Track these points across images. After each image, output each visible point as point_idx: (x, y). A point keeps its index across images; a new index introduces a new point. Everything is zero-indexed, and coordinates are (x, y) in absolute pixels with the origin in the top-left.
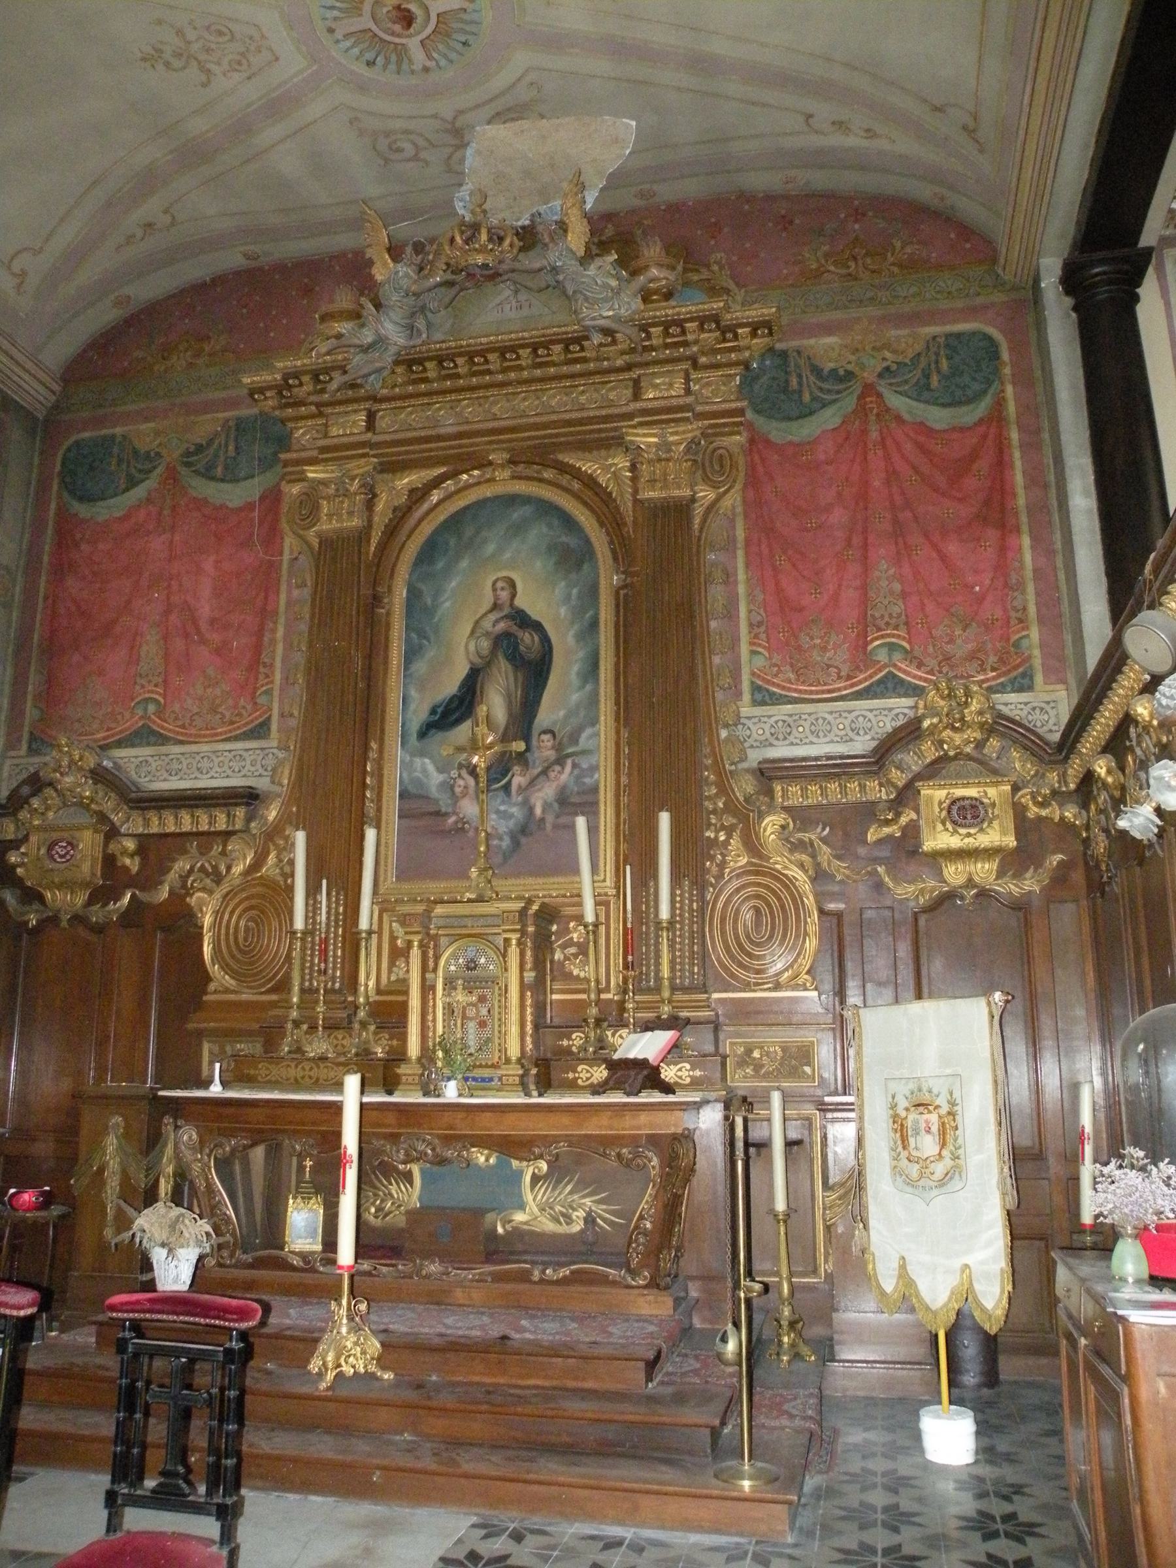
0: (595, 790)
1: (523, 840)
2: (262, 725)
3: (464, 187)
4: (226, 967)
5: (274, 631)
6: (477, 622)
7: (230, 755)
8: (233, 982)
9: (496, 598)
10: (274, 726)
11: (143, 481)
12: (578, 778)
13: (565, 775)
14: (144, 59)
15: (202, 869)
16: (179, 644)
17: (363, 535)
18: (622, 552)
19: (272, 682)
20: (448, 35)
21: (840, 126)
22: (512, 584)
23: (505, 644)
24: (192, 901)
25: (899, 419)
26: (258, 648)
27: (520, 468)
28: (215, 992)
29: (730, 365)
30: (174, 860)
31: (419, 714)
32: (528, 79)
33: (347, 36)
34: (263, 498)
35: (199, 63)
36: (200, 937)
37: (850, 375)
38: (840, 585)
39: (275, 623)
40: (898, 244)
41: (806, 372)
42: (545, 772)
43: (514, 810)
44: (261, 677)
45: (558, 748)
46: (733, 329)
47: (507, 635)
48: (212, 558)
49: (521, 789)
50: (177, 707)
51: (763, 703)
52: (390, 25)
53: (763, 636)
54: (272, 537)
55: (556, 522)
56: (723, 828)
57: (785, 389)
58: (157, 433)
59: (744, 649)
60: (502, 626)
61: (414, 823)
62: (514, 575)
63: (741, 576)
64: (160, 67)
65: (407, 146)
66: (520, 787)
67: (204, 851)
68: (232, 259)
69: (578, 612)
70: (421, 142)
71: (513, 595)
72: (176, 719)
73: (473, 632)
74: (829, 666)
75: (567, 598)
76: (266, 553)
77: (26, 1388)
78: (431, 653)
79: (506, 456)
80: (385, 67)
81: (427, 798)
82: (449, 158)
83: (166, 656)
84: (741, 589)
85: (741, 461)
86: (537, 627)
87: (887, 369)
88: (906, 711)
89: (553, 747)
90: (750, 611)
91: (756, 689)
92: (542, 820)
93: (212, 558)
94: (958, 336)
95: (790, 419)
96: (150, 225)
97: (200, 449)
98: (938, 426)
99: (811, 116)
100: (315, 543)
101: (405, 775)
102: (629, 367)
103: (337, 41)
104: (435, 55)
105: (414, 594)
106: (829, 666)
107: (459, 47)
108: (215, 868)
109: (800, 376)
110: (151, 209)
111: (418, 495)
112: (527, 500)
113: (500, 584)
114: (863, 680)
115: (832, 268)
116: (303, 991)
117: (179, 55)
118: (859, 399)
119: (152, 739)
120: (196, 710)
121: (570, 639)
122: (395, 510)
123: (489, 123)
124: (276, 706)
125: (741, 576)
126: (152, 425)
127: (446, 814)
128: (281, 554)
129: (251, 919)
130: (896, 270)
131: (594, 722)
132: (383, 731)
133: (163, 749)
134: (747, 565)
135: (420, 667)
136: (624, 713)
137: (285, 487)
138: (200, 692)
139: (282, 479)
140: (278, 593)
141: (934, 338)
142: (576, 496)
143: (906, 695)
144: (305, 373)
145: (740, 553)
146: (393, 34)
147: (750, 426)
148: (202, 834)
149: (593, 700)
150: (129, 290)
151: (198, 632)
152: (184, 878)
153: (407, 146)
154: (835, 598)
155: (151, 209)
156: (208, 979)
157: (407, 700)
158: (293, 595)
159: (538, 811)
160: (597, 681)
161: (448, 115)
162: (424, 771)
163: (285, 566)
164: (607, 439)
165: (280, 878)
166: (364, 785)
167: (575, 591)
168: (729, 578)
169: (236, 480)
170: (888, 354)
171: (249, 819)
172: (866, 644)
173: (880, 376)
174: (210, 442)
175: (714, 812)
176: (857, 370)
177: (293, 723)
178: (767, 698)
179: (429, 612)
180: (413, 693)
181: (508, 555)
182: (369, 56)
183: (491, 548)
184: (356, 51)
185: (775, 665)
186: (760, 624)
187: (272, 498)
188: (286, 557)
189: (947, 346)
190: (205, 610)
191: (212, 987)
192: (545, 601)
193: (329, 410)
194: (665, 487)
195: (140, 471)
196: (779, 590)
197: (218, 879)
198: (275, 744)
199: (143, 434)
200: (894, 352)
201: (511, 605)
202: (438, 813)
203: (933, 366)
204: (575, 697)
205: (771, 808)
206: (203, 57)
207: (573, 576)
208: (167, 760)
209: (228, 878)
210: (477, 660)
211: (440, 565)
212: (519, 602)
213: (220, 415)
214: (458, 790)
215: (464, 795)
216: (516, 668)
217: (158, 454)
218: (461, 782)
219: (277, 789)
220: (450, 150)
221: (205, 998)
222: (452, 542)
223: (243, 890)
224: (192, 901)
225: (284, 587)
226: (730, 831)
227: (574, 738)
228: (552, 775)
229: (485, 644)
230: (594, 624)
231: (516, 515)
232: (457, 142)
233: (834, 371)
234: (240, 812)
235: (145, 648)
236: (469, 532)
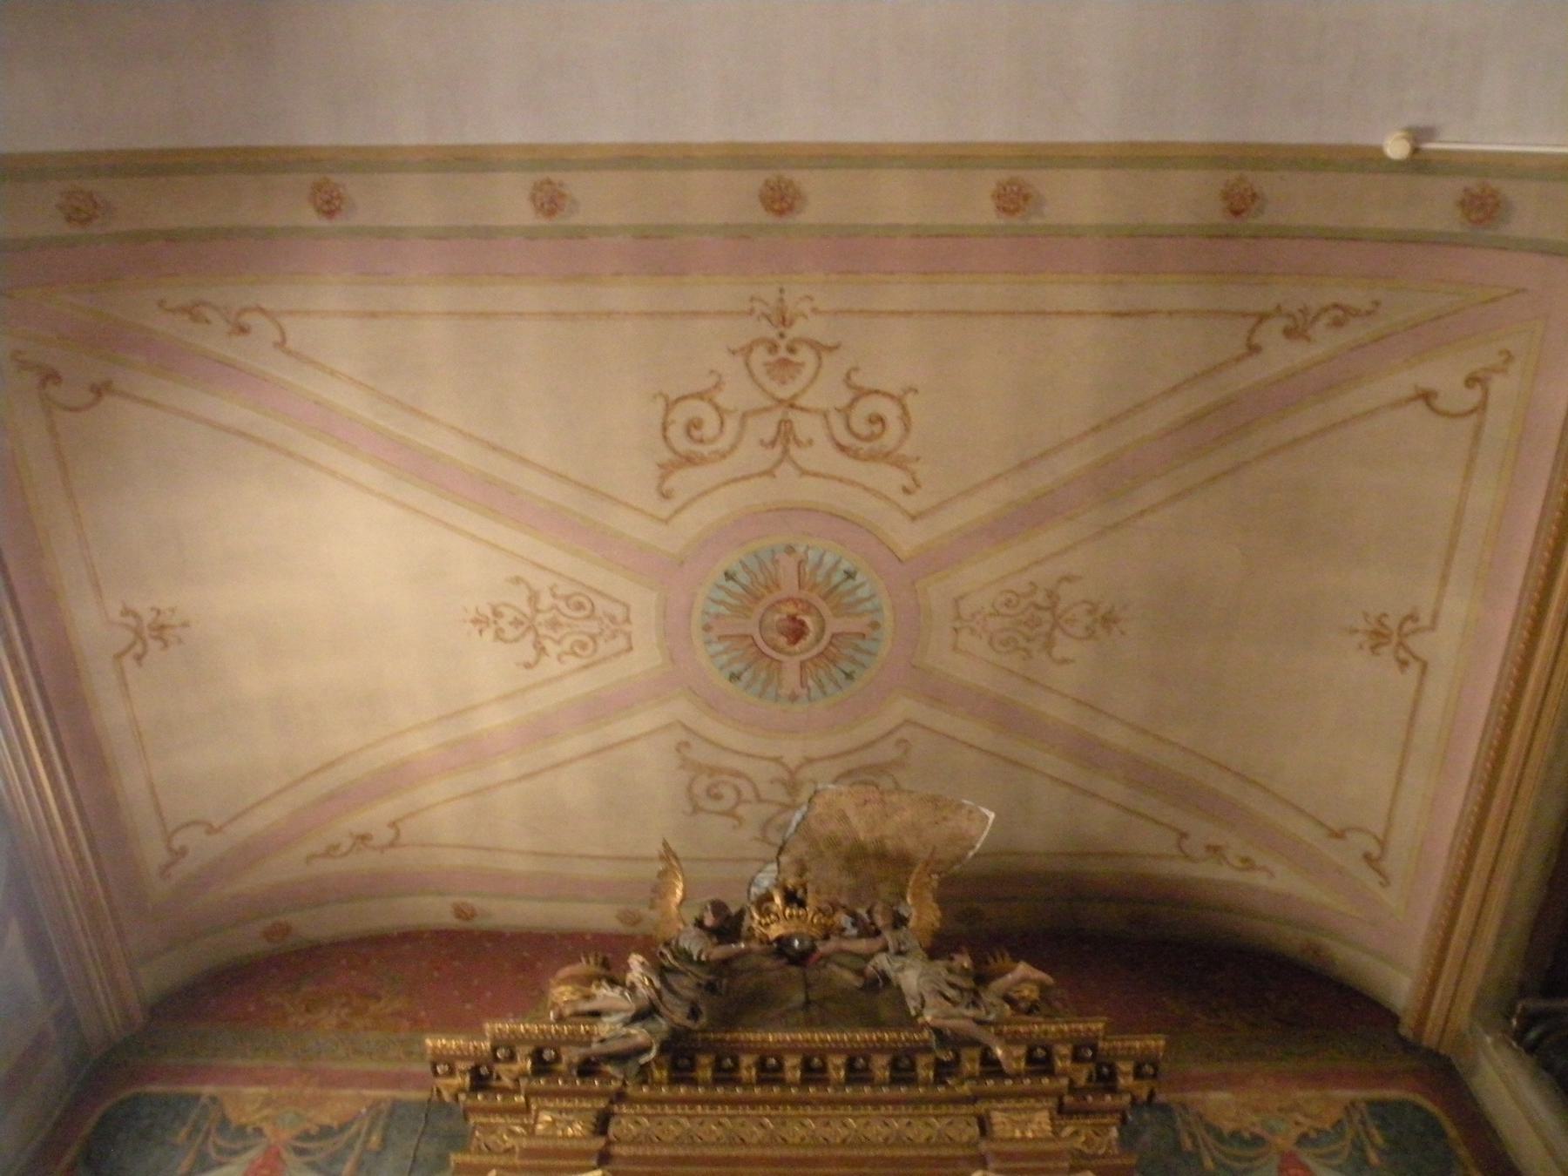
11: (221, 1164)
14: (475, 621)
20: (834, 662)
32: (898, 736)
33: (721, 638)
35: (537, 635)
37: (1257, 1141)
41: (1200, 1132)
52: (775, 635)
57: (1177, 1147)
64: (489, 634)
65: (728, 793)
70: (748, 793)
77: (143, 146)
80: (748, 686)
96: (364, 838)
97: (326, 1132)
102: (973, 1099)
103: (708, 643)
104: (811, 683)
107: (840, 677)
109: (1192, 1136)
117: (516, 623)
123: (835, 781)
126: (263, 1090)
141: (1353, 1104)
146: (775, 648)
153: (728, 793)
170: (1301, 1119)
174: (343, 1128)
176: (1265, 1134)
182: (737, 667)
184: (725, 658)
195: (220, 1151)
203: (1363, 1136)
206: (542, 631)
213: (366, 1092)
217: (259, 1131)
220: (773, 809)
232: (787, 800)
233: (1235, 1135)
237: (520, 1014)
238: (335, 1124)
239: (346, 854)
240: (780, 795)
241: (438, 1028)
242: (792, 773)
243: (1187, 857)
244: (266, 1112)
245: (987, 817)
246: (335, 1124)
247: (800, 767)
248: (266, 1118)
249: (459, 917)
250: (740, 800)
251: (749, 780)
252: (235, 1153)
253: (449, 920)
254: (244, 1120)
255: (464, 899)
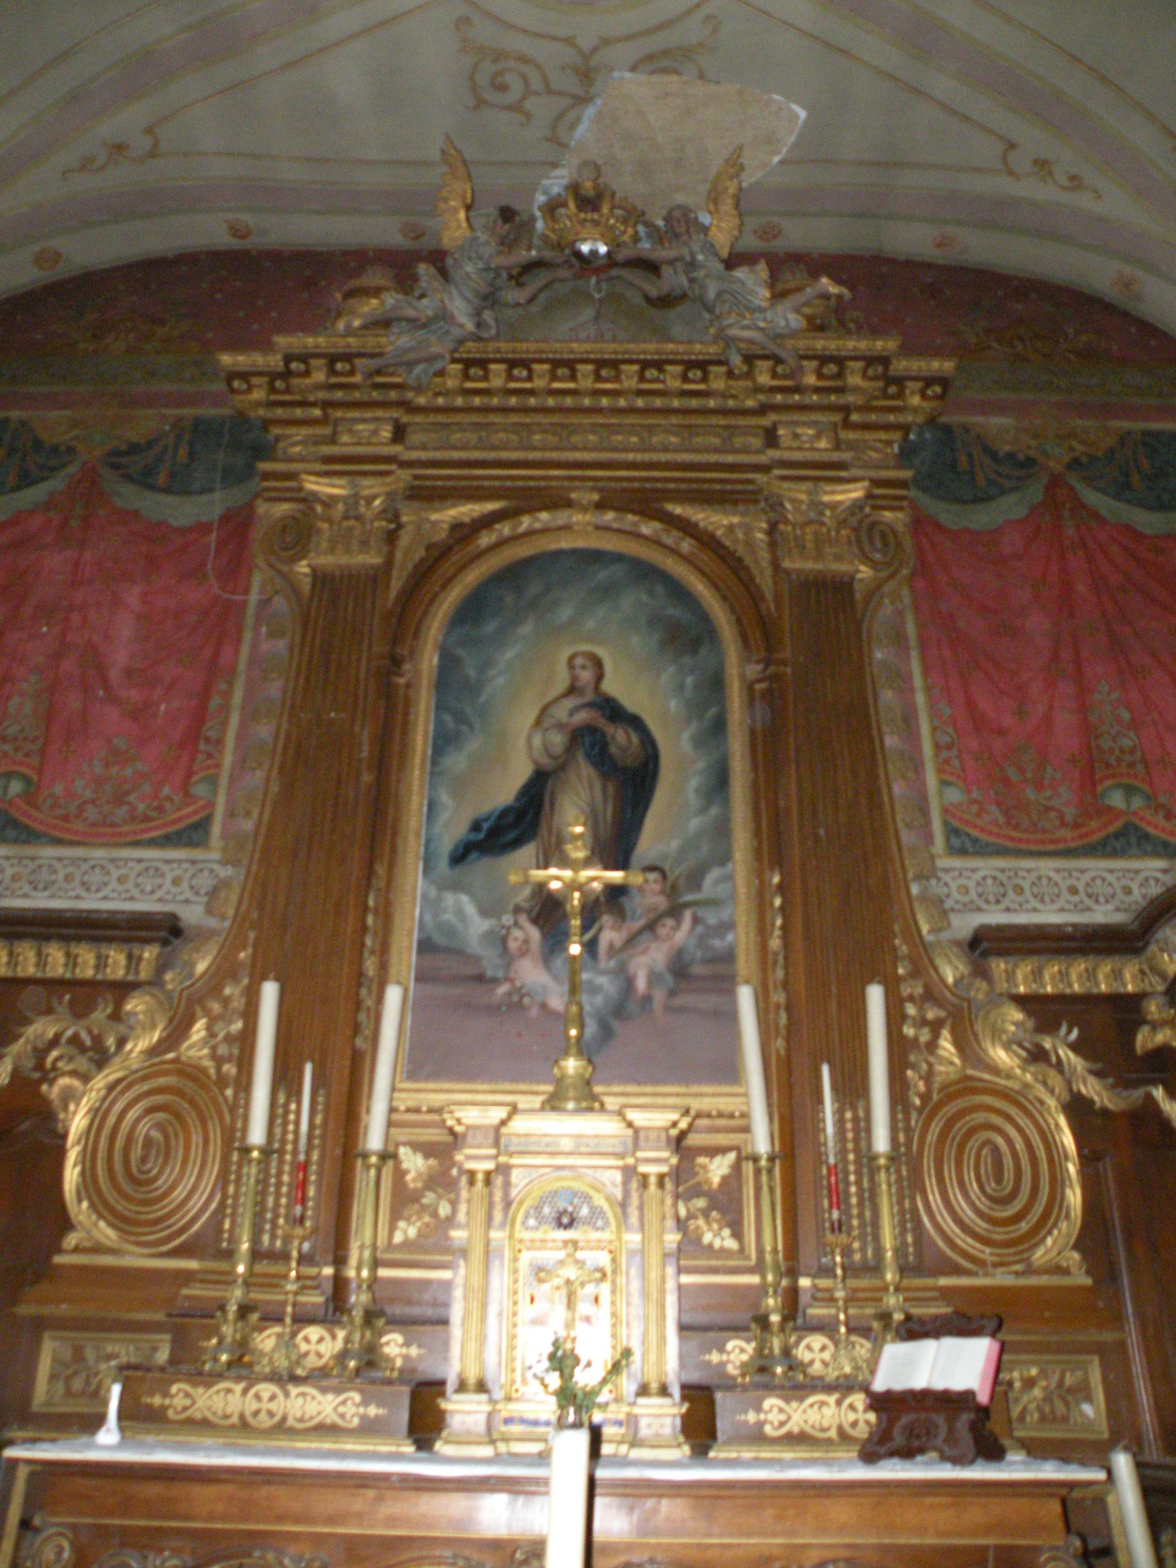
0: (729, 957)
1: (616, 1025)
2: (195, 826)
3: (559, 172)
4: (102, 1207)
5: (227, 695)
6: (544, 710)
7: (139, 867)
8: (111, 1233)
9: (574, 678)
10: (216, 829)
11: (43, 479)
12: (702, 938)
13: (682, 934)
15: (75, 1040)
16: (73, 702)
17: (378, 577)
18: (760, 631)
19: (218, 766)
21: (1043, 166)
22: (598, 664)
23: (588, 742)
24: (53, 1092)
25: (1096, 515)
26: (200, 716)
27: (609, 516)
28: (77, 1250)
29: (886, 427)
30: (27, 1022)
31: (453, 828)
34: (225, 519)
36: (60, 1154)
37: (1030, 462)
38: (1051, 707)
39: (231, 684)
40: (1071, 331)
42: (651, 927)
43: (603, 980)
44: (200, 757)
45: (672, 891)
46: (900, 381)
47: (590, 729)
48: (137, 589)
49: (612, 950)
50: (58, 789)
51: (962, 852)
53: (956, 763)
54: (235, 569)
55: (659, 589)
56: (924, 1022)
57: (953, 468)
58: (75, 424)
59: (931, 779)
60: (582, 717)
61: (441, 990)
62: (600, 651)
63: (918, 681)
65: (516, 86)
66: (611, 946)
67: (80, 1011)
68: (207, 231)
69: (695, 708)
70: (536, 84)
71: (600, 677)
72: (55, 806)
73: (538, 722)
74: (1048, 809)
75: (681, 687)
76: (224, 589)
78: (473, 745)
79: (596, 497)
81: (460, 952)
82: (561, 115)
83: (49, 718)
84: (920, 699)
85: (907, 541)
86: (636, 722)
87: (1076, 461)
88: (1159, 875)
89: (662, 892)
90: (934, 729)
91: (951, 832)
92: (647, 999)
93: (137, 589)
94: (1156, 434)
95: (964, 502)
96: (120, 147)
97: (134, 448)
98: (1147, 531)
99: (1012, 146)
100: (306, 586)
101: (428, 918)
102: (763, 410)
105: (449, 664)
106: (1048, 809)
108: (98, 1040)
109: (970, 455)
110: (128, 121)
111: (463, 532)
112: (618, 558)
113: (579, 661)
114: (1097, 830)
115: (994, 344)
116: (256, 1255)
118: (1047, 488)
119: (10, 833)
120: (88, 794)
121: (686, 746)
122: (429, 547)
123: (633, 69)
124: (221, 800)
125: (918, 681)
126: (68, 413)
127: (495, 981)
128: (246, 591)
129: (159, 1126)
130: (1072, 357)
131: (724, 858)
132: (393, 850)
133: (30, 851)
134: (926, 672)
135: (456, 762)
136: (772, 848)
137: (262, 508)
138: (99, 769)
139: (257, 495)
140: (238, 642)
142: (686, 559)
143: (1155, 854)
144: (318, 356)
145: (914, 654)
147: (913, 505)
148: (83, 983)
149: (722, 830)
150: (60, 243)
151: (105, 683)
152: (40, 1054)
153: (516, 86)
154: (1048, 720)
155: (128, 121)
156: (65, 1224)
157: (435, 808)
158: (264, 650)
159: (641, 984)
160: (726, 801)
161: (586, 42)
162: (460, 913)
163: (251, 610)
164: (733, 492)
165: (208, 1064)
166: (364, 929)
167: (689, 680)
168: (902, 680)
169: (188, 493)
170: (1074, 444)
171: (162, 966)
172: (1094, 784)
173: (1069, 467)
174: (150, 445)
175: (911, 998)
177: (248, 825)
178: (968, 845)
179: (473, 689)
180: (444, 797)
181: (590, 624)
183: (565, 613)
185: (975, 801)
186: (949, 747)
187: (238, 524)
188: (254, 597)
189: (1145, 444)
190: (119, 658)
191: (71, 1240)
192: (647, 689)
193: (339, 414)
194: (819, 556)
196: (970, 704)
197: (101, 1059)
198: (215, 855)
199: (53, 423)
200: (1082, 442)
201: (597, 688)
202: (480, 978)
204: (694, 824)
205: (996, 999)
207: (687, 660)
208: (32, 866)
209: (117, 1060)
210: (545, 761)
211: (490, 627)
212: (610, 686)
214: (513, 945)
215: (523, 952)
216: (604, 776)
217: (71, 450)
218: (517, 933)
219: (212, 923)
220: (566, 102)
221: (58, 1259)
222: (509, 599)
223: (145, 1078)
224: (53, 1092)
225: (248, 636)
226: (936, 1027)
227: (695, 879)
228: (662, 931)
229: (558, 740)
230: (719, 727)
231: (602, 575)
232: (578, 90)
233: (1011, 456)
234: (149, 953)
235: (15, 701)
236: (534, 588)
237: (309, 330)
238: (143, 441)
239: (102, 168)
240: (572, 85)
241: (234, 346)
242: (587, 57)
243: (1011, 173)
244: (75, 432)
245: (797, 116)
246: (143, 441)
247: (595, 49)
248: (77, 438)
249: (235, 236)
250: (528, 92)
251: (537, 66)
252: (54, 469)
253: (223, 240)
254: (55, 440)
255: (238, 216)
